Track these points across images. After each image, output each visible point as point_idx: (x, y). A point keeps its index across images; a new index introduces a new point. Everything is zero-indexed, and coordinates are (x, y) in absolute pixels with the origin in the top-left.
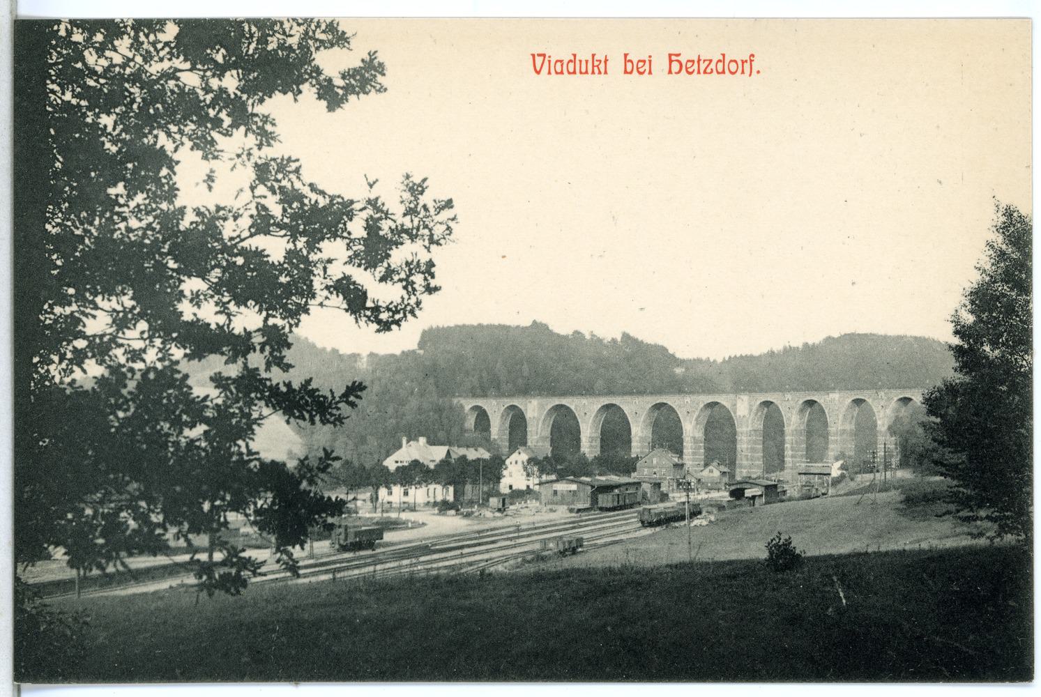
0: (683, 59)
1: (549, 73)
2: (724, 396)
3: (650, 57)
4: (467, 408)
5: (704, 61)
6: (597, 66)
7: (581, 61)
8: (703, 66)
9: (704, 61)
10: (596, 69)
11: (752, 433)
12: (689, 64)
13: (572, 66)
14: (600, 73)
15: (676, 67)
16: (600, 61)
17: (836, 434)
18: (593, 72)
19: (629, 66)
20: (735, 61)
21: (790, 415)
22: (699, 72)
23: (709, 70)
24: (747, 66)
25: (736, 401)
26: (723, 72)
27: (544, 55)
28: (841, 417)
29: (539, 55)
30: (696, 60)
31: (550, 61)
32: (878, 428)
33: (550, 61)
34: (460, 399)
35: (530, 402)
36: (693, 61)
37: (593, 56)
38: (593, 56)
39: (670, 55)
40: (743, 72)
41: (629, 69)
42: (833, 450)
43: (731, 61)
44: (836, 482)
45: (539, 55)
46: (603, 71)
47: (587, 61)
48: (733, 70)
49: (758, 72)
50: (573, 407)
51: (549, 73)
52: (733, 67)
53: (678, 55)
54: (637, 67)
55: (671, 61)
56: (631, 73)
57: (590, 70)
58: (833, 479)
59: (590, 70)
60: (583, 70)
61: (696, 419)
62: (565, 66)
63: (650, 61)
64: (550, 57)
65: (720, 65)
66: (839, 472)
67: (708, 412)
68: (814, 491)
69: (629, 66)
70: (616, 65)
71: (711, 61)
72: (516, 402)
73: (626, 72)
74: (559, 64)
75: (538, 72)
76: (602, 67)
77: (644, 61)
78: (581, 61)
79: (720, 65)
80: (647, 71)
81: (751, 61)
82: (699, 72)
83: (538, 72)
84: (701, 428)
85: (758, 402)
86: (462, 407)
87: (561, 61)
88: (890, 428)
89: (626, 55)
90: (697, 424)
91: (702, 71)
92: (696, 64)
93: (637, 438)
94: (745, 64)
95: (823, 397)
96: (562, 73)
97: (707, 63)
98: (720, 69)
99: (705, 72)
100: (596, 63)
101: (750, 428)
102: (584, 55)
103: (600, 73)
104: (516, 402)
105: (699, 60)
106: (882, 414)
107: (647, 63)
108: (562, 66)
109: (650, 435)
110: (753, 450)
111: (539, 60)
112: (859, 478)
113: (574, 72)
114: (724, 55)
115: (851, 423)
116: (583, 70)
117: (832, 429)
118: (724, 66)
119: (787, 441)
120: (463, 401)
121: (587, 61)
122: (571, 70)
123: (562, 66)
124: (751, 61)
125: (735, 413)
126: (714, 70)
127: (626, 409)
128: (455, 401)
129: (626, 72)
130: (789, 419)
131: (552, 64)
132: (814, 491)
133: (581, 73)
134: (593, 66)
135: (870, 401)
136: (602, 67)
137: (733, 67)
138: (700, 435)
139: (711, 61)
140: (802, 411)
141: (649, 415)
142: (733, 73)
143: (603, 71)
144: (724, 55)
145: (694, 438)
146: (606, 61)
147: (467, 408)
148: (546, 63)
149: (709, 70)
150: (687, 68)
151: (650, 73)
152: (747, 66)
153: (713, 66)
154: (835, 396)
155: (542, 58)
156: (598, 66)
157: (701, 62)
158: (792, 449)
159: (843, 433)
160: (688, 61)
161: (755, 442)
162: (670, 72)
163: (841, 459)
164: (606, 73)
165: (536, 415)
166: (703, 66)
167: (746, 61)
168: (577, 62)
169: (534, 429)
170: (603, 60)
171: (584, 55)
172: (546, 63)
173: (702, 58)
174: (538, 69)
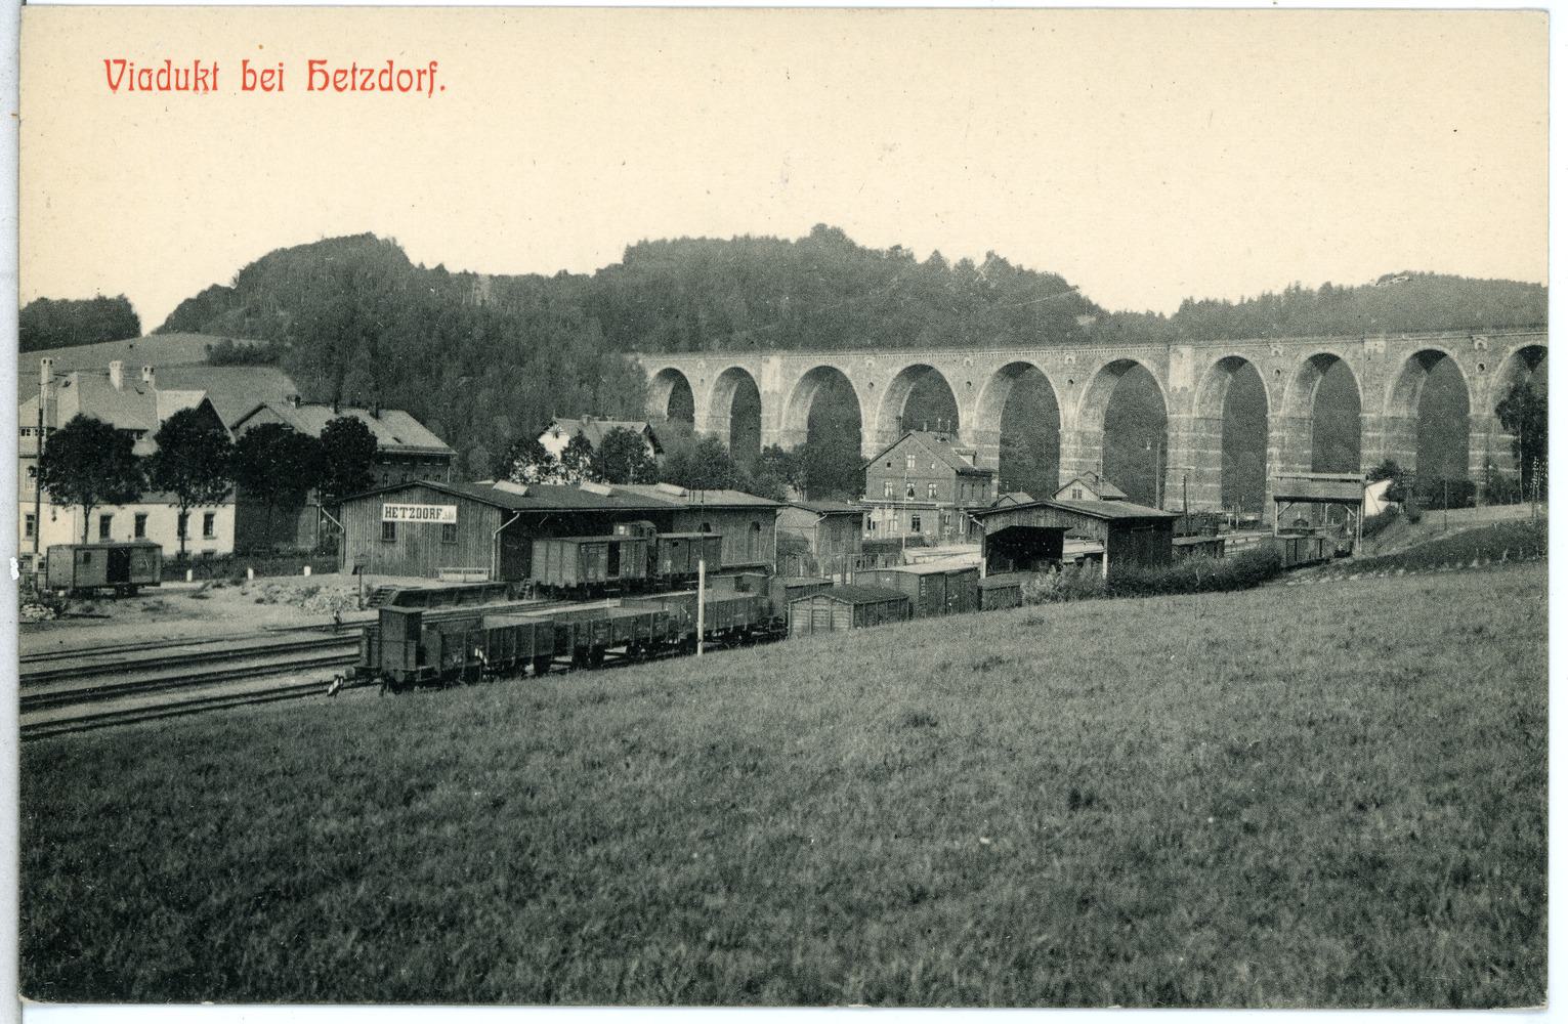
0: (330, 69)
1: (131, 88)
2: (1144, 348)
3: (281, 65)
4: (652, 374)
5: (362, 71)
6: (203, 79)
7: (178, 71)
8: (360, 79)
9: (362, 71)
10: (200, 83)
11: (1202, 423)
12: (340, 76)
13: (164, 79)
14: (206, 88)
15: (319, 79)
16: (207, 71)
17: (1376, 425)
18: (196, 88)
19: (250, 78)
20: (409, 72)
21: (1278, 385)
22: (354, 88)
23: (368, 85)
24: (426, 79)
25: (1167, 355)
26: (390, 88)
27: (123, 62)
28: (1389, 388)
29: (116, 62)
30: (350, 69)
31: (132, 71)
32: (1472, 412)
33: (132, 71)
34: (640, 355)
35: (768, 362)
36: (345, 72)
37: (197, 63)
38: (197, 63)
39: (311, 63)
40: (419, 88)
41: (249, 84)
42: (1370, 459)
43: (402, 72)
44: (1374, 528)
45: (116, 62)
46: (210, 83)
47: (187, 71)
48: (405, 85)
49: (443, 88)
50: (847, 372)
51: (131, 88)
52: (405, 80)
53: (323, 62)
54: (260, 80)
55: (312, 72)
56: (253, 88)
57: (192, 86)
58: (1368, 520)
59: (192, 86)
60: (182, 84)
61: (1088, 396)
62: (154, 78)
63: (281, 71)
64: (131, 64)
65: (386, 78)
66: (1382, 505)
67: (1113, 382)
68: (1312, 545)
69: (250, 78)
70: (230, 77)
71: (372, 71)
72: (744, 362)
73: (245, 87)
74: (145, 76)
75: (114, 88)
76: (209, 81)
77: (272, 72)
78: (178, 71)
79: (386, 78)
80: (277, 86)
81: (432, 71)
82: (354, 88)
83: (114, 88)
84: (1098, 412)
85: (1215, 360)
86: (641, 372)
87: (149, 71)
88: (1500, 410)
89: (245, 63)
90: (1089, 405)
91: (358, 86)
92: (350, 75)
93: (970, 434)
94: (423, 76)
95: (1354, 347)
96: (149, 88)
97: (366, 74)
98: (386, 84)
99: (363, 88)
100: (201, 74)
101: (1196, 414)
102: (182, 62)
103: (206, 88)
104: (744, 362)
105: (354, 70)
106: (1480, 384)
107: (277, 74)
108: (150, 77)
109: (998, 429)
110: (1201, 459)
111: (116, 69)
112: (1434, 518)
113: (168, 88)
114: (391, 63)
115: (1410, 404)
116: (182, 84)
117: (1369, 416)
118: (391, 79)
119: (1271, 441)
120: (642, 360)
121: (187, 71)
122: (163, 84)
123: (150, 77)
124: (432, 71)
125: (1166, 384)
126: (377, 85)
127: (948, 373)
128: (630, 357)
129: (245, 87)
130: (1278, 395)
131: (136, 75)
132: (1312, 545)
133: (178, 88)
134: (196, 79)
135: (1452, 354)
136: (209, 81)
137: (405, 80)
138: (1095, 428)
139: (372, 71)
140: (1305, 379)
141: (993, 387)
142: (404, 90)
143: (210, 83)
144: (391, 63)
145: (1082, 434)
146: (216, 70)
147: (652, 374)
148: (127, 74)
149: (368, 85)
150: (335, 82)
151: (281, 88)
152: (426, 79)
153: (374, 79)
154: (1377, 345)
155: (120, 66)
156: (203, 79)
157: (358, 73)
158: (1283, 458)
159: (1394, 426)
160: (338, 71)
161: (1205, 444)
162: (311, 88)
163: (1385, 477)
164: (215, 88)
165: (778, 388)
166: (360, 79)
167: (425, 72)
168: (173, 72)
169: (775, 414)
170: (211, 70)
171: (182, 62)
172: (127, 74)
173: (359, 67)
174: (114, 83)
